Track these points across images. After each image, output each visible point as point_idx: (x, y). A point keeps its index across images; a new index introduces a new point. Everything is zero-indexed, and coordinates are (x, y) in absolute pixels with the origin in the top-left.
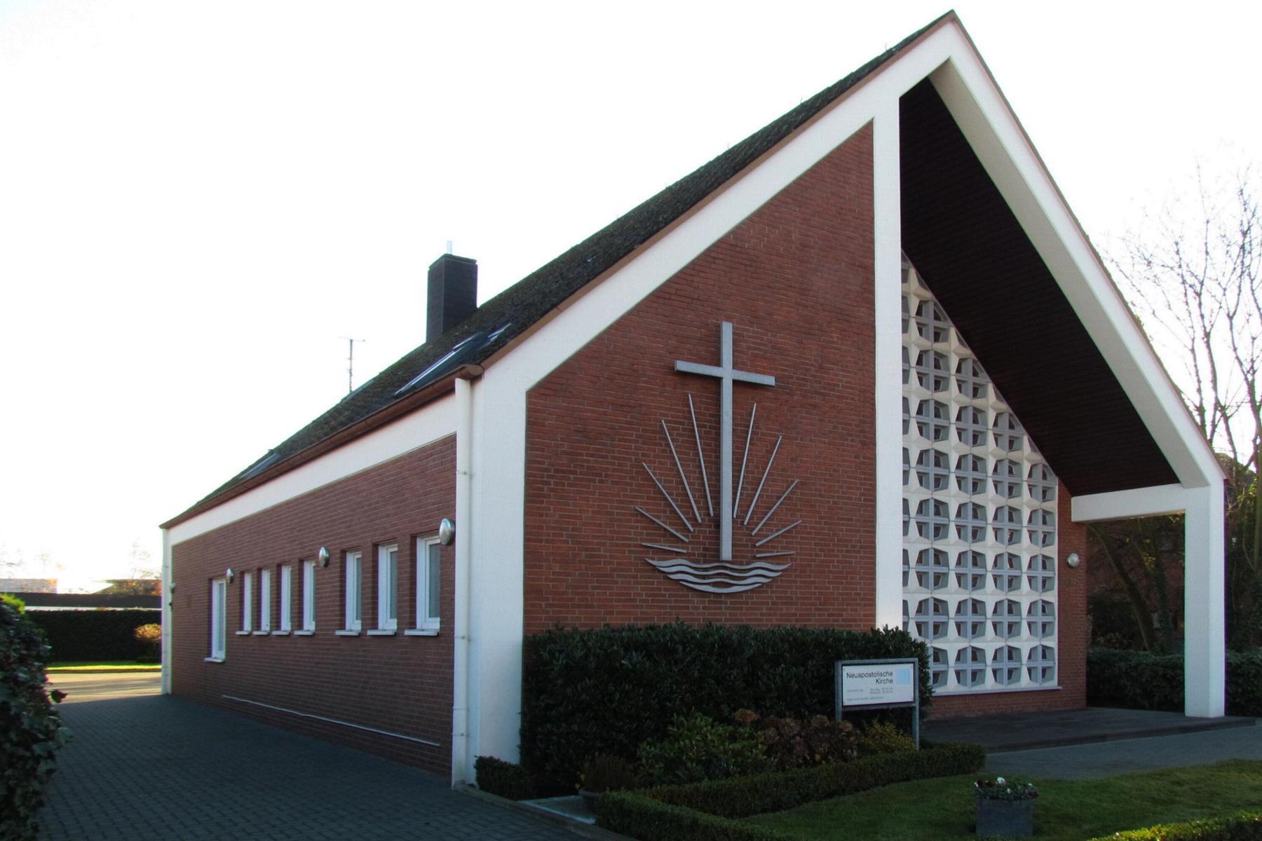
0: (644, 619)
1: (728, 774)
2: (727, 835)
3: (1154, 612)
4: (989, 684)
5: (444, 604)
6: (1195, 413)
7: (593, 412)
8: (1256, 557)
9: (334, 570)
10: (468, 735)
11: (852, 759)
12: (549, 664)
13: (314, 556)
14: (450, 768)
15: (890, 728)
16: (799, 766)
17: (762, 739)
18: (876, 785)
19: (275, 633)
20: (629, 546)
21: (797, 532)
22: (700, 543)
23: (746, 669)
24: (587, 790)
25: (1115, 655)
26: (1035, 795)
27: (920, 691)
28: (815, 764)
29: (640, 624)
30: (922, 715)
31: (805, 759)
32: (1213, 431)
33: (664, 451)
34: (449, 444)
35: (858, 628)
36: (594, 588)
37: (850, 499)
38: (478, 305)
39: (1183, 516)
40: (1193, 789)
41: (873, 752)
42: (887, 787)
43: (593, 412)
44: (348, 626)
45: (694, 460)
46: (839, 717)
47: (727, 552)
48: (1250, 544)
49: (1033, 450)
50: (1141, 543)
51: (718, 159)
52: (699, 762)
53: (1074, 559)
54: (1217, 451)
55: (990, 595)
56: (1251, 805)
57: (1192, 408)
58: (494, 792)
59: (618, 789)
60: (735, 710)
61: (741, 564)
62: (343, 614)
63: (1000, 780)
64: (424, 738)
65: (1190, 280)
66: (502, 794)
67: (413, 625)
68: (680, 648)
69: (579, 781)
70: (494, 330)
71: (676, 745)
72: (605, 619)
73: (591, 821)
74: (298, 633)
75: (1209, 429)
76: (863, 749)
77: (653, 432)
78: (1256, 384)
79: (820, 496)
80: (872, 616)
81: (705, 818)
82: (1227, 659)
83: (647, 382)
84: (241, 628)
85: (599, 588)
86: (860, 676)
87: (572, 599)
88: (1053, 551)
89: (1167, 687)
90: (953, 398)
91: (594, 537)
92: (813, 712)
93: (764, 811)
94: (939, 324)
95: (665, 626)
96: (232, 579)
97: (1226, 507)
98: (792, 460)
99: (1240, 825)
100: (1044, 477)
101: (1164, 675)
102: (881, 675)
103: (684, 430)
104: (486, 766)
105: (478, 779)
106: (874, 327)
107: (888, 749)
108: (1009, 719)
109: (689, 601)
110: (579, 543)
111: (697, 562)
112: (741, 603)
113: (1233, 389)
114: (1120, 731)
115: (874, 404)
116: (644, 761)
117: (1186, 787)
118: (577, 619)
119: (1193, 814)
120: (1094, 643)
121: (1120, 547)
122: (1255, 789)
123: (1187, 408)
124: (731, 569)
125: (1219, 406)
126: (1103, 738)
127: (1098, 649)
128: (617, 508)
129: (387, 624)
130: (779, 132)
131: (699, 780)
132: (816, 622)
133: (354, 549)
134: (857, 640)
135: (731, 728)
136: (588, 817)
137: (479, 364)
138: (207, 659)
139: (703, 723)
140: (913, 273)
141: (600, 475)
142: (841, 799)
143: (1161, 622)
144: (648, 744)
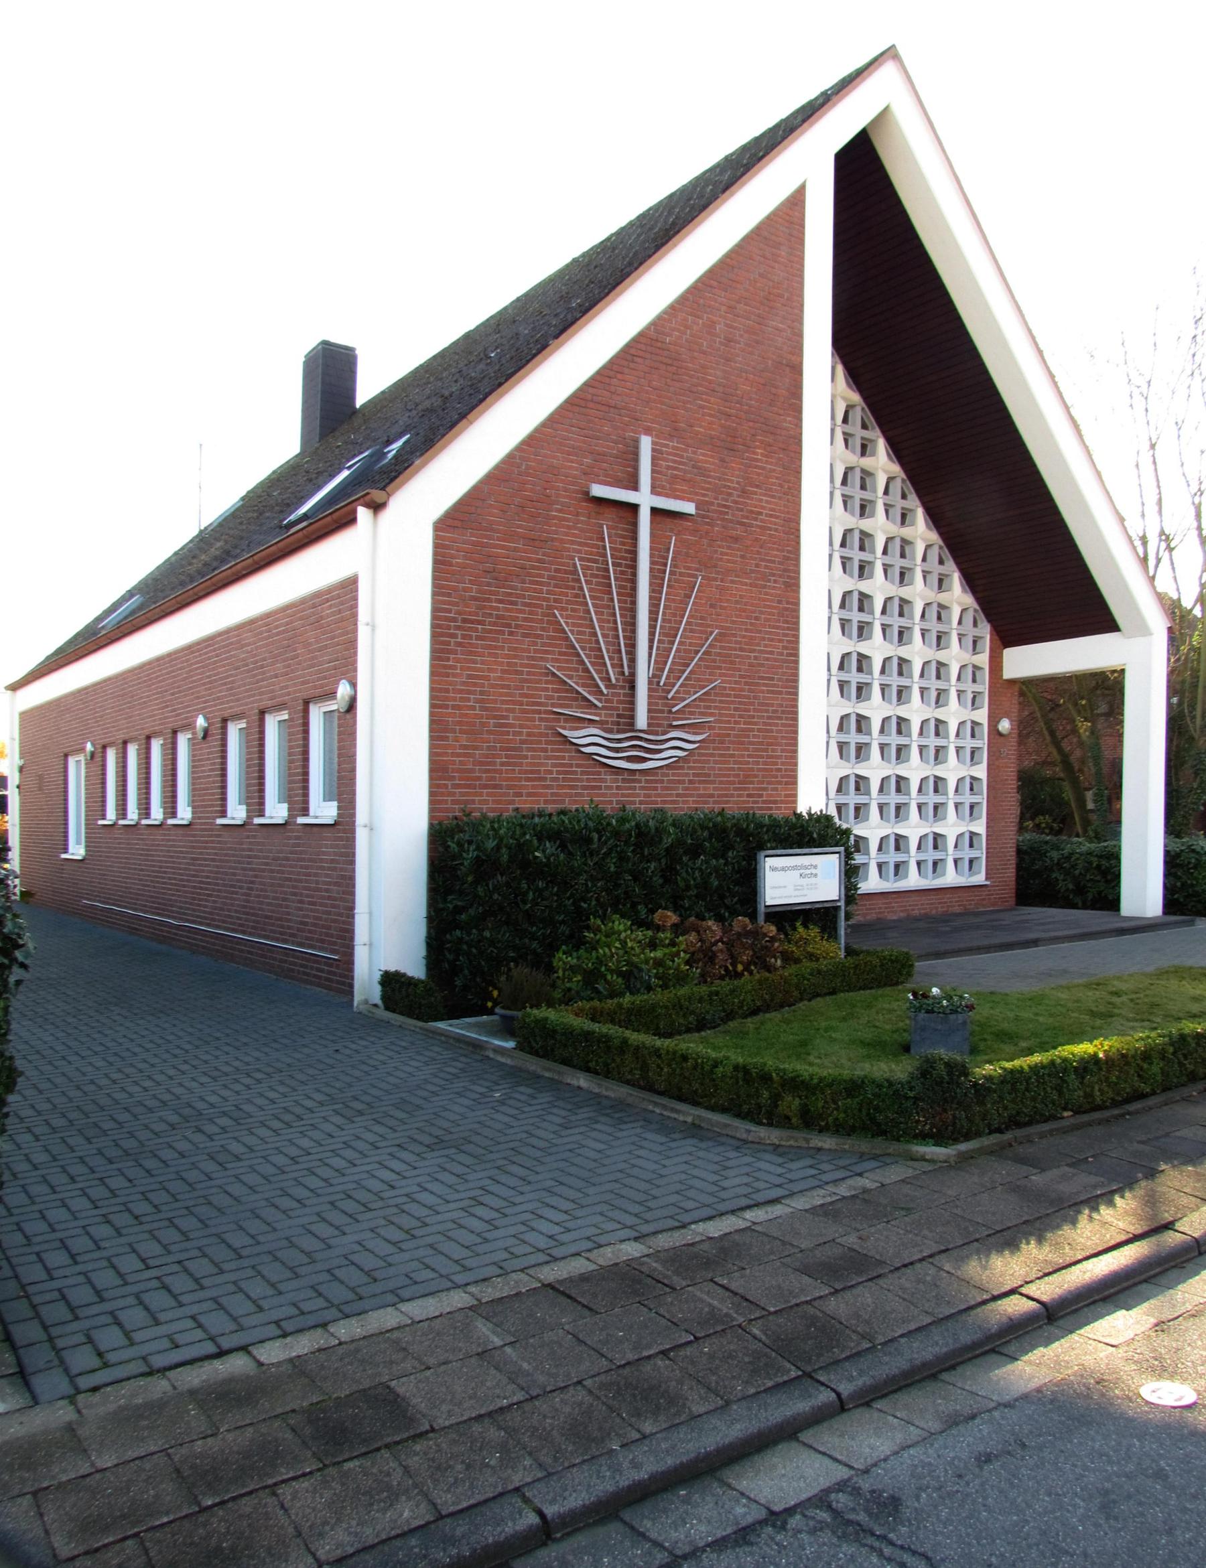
0: (554, 802)
1: (649, 989)
2: (659, 1056)
3: (1089, 789)
4: (913, 880)
5: (343, 786)
6: (1138, 543)
7: (503, 547)
8: (1198, 721)
9: (214, 742)
10: (371, 945)
11: (776, 969)
12: (461, 862)
13: (190, 726)
14: (351, 986)
15: (814, 931)
16: (722, 978)
17: (683, 947)
18: (801, 1000)
19: (144, 822)
20: (539, 712)
21: (716, 695)
22: (612, 709)
23: (663, 861)
24: (503, 1008)
25: (1047, 842)
26: (971, 1007)
27: (846, 887)
28: (738, 975)
29: (550, 808)
30: (848, 917)
31: (726, 969)
32: (1157, 566)
33: (577, 596)
34: (349, 587)
35: (780, 813)
36: (502, 764)
37: (771, 653)
38: (358, 404)
39: (1123, 671)
40: (1132, 1000)
41: (797, 961)
42: (813, 1003)
43: (503, 547)
44: (229, 814)
45: (608, 607)
46: (761, 919)
47: (642, 721)
48: (1192, 707)
49: (964, 591)
50: (1076, 704)
51: (631, 224)
52: (620, 974)
53: (1005, 725)
54: (1159, 590)
55: (915, 770)
56: (1194, 1016)
57: (1134, 537)
58: (401, 1013)
59: (538, 1006)
60: (652, 911)
61: (657, 734)
62: (224, 799)
63: (935, 991)
64: (321, 949)
65: (1138, 380)
66: (410, 1016)
67: (305, 811)
68: (595, 836)
69: (491, 998)
70: (389, 442)
71: (594, 954)
72: (513, 802)
73: (510, 1044)
74: (171, 822)
75: (1152, 562)
76: (788, 958)
77: (566, 572)
78: (1203, 508)
79: (741, 650)
80: (793, 797)
81: (635, 1037)
82: (1165, 846)
83: (560, 511)
84: (104, 817)
85: (508, 764)
86: (783, 869)
87: (479, 778)
88: (982, 715)
89: (1099, 884)
90: (880, 526)
91: (503, 702)
92: (734, 913)
93: (688, 1031)
94: (867, 434)
95: (577, 810)
96: (93, 755)
97: (1169, 660)
98: (712, 606)
99: (1183, 1037)
100: (975, 624)
101: (1099, 867)
102: (806, 868)
103: (598, 569)
104: (391, 981)
105: (384, 997)
106: (800, 441)
107: (812, 957)
108: (943, 921)
109: (601, 780)
110: (486, 709)
111: (610, 731)
112: (656, 781)
113: (1180, 520)
114: (1056, 934)
115: (798, 537)
116: (560, 973)
117: (1124, 998)
118: (485, 804)
119: (1133, 1028)
120: (1021, 829)
121: (1052, 709)
122: (1196, 999)
123: (1130, 538)
124: (647, 740)
125: (1165, 537)
126: (1035, 943)
127: (1028, 836)
128: (527, 666)
129: (276, 811)
130: (701, 196)
131: (622, 995)
132: (736, 803)
133: (237, 717)
134: (780, 827)
135: (650, 933)
136: (507, 1041)
137: (383, 489)
138: (64, 856)
139: (622, 927)
140: (840, 369)
141: (509, 626)
142: (767, 1015)
143: (1095, 801)
144: (564, 953)
